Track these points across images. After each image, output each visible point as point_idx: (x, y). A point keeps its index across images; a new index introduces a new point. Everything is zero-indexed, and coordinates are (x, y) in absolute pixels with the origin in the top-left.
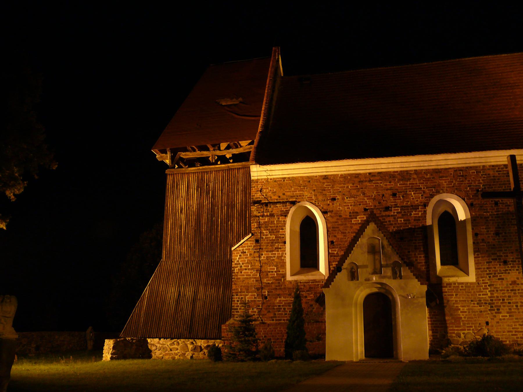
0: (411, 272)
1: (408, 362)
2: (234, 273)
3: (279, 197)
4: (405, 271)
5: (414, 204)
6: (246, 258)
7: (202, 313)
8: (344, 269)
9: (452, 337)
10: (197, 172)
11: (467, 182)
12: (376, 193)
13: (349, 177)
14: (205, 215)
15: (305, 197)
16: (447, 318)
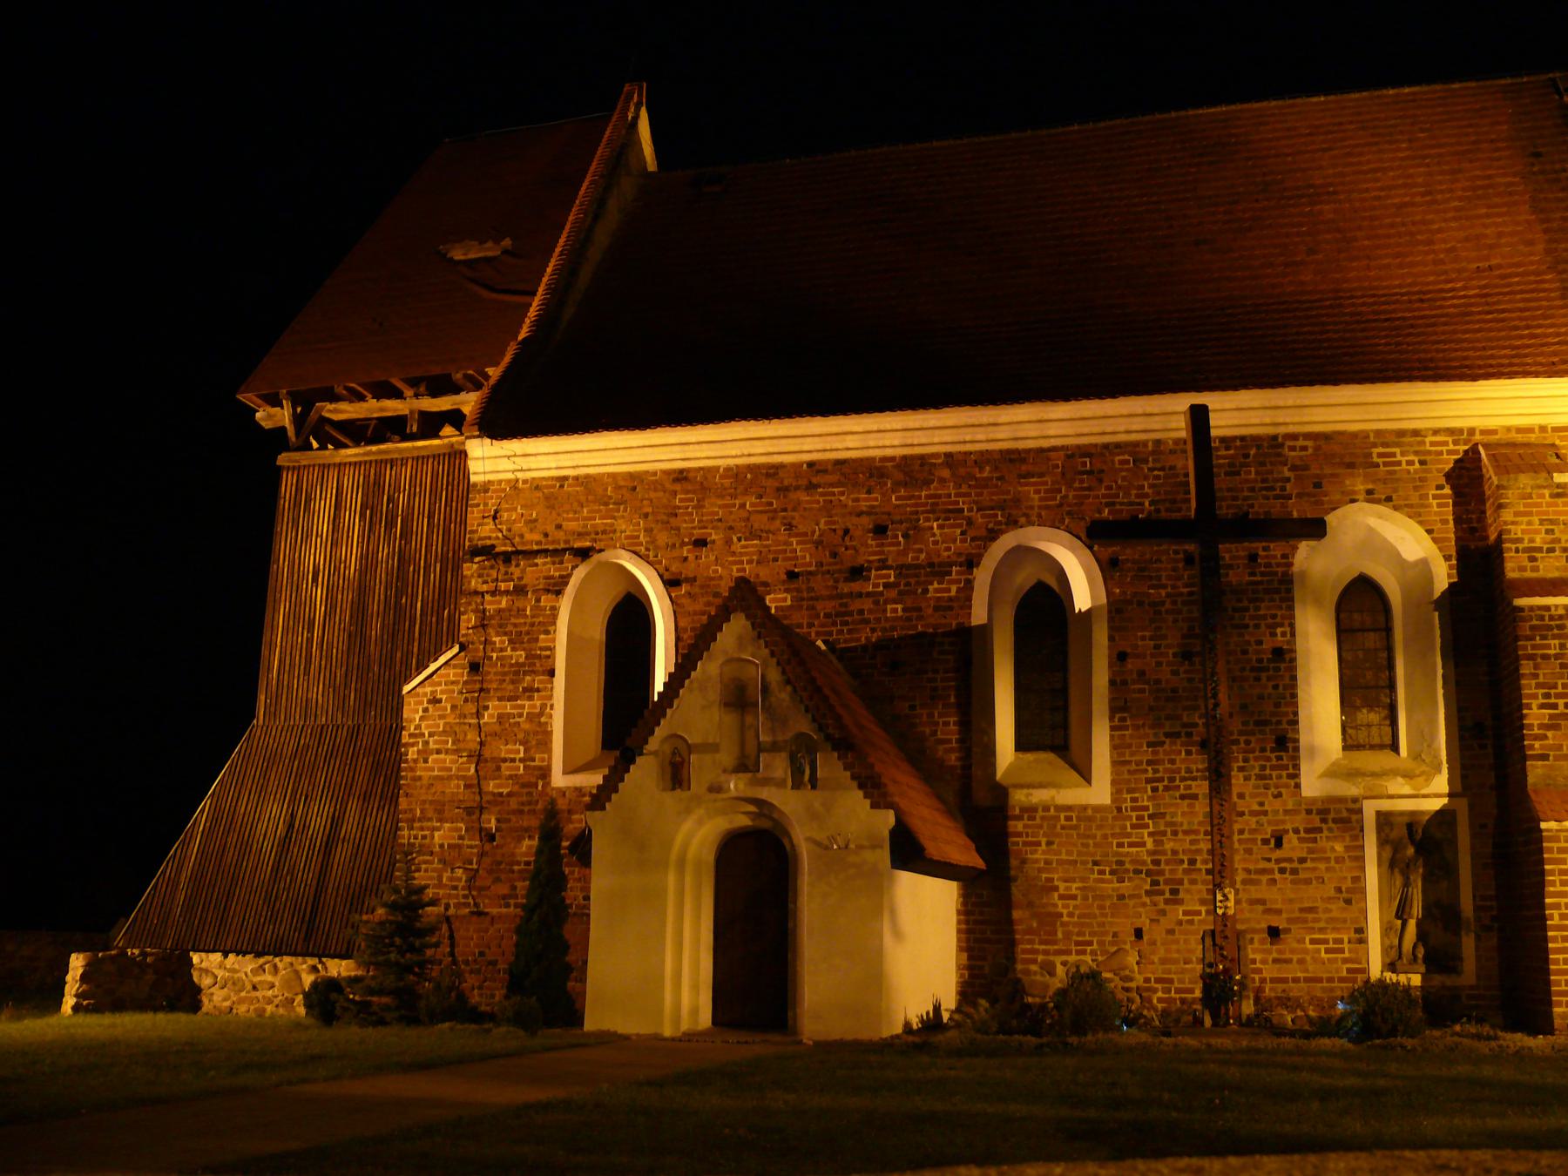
0: (845, 769)
1: (811, 1043)
2: (406, 761)
3: (546, 535)
4: (829, 766)
5: (936, 560)
6: (441, 717)
7: (348, 882)
8: (650, 753)
9: (1027, 972)
10: (366, 462)
11: (1103, 491)
12: (827, 523)
13: (749, 476)
14: (379, 591)
15: (619, 534)
16: (1016, 914)
